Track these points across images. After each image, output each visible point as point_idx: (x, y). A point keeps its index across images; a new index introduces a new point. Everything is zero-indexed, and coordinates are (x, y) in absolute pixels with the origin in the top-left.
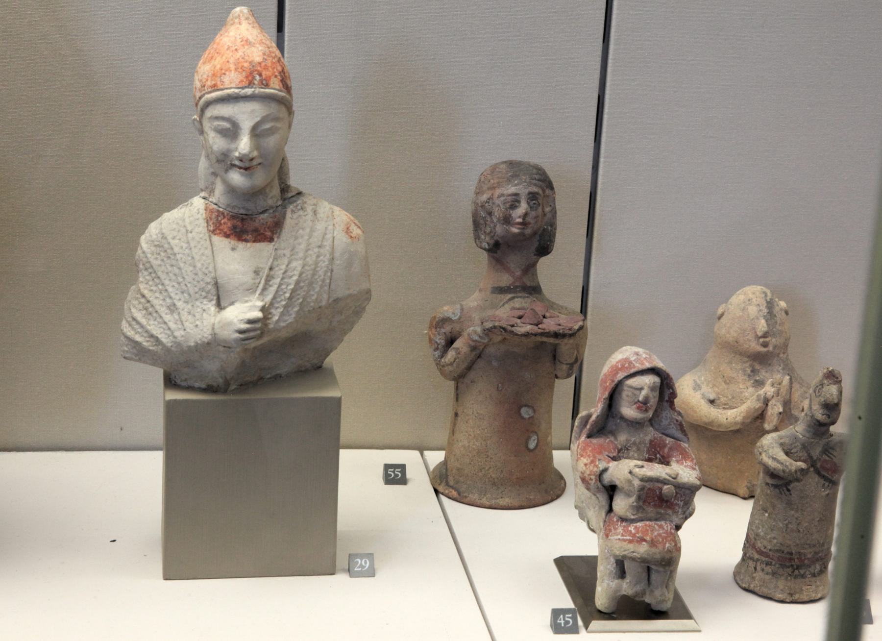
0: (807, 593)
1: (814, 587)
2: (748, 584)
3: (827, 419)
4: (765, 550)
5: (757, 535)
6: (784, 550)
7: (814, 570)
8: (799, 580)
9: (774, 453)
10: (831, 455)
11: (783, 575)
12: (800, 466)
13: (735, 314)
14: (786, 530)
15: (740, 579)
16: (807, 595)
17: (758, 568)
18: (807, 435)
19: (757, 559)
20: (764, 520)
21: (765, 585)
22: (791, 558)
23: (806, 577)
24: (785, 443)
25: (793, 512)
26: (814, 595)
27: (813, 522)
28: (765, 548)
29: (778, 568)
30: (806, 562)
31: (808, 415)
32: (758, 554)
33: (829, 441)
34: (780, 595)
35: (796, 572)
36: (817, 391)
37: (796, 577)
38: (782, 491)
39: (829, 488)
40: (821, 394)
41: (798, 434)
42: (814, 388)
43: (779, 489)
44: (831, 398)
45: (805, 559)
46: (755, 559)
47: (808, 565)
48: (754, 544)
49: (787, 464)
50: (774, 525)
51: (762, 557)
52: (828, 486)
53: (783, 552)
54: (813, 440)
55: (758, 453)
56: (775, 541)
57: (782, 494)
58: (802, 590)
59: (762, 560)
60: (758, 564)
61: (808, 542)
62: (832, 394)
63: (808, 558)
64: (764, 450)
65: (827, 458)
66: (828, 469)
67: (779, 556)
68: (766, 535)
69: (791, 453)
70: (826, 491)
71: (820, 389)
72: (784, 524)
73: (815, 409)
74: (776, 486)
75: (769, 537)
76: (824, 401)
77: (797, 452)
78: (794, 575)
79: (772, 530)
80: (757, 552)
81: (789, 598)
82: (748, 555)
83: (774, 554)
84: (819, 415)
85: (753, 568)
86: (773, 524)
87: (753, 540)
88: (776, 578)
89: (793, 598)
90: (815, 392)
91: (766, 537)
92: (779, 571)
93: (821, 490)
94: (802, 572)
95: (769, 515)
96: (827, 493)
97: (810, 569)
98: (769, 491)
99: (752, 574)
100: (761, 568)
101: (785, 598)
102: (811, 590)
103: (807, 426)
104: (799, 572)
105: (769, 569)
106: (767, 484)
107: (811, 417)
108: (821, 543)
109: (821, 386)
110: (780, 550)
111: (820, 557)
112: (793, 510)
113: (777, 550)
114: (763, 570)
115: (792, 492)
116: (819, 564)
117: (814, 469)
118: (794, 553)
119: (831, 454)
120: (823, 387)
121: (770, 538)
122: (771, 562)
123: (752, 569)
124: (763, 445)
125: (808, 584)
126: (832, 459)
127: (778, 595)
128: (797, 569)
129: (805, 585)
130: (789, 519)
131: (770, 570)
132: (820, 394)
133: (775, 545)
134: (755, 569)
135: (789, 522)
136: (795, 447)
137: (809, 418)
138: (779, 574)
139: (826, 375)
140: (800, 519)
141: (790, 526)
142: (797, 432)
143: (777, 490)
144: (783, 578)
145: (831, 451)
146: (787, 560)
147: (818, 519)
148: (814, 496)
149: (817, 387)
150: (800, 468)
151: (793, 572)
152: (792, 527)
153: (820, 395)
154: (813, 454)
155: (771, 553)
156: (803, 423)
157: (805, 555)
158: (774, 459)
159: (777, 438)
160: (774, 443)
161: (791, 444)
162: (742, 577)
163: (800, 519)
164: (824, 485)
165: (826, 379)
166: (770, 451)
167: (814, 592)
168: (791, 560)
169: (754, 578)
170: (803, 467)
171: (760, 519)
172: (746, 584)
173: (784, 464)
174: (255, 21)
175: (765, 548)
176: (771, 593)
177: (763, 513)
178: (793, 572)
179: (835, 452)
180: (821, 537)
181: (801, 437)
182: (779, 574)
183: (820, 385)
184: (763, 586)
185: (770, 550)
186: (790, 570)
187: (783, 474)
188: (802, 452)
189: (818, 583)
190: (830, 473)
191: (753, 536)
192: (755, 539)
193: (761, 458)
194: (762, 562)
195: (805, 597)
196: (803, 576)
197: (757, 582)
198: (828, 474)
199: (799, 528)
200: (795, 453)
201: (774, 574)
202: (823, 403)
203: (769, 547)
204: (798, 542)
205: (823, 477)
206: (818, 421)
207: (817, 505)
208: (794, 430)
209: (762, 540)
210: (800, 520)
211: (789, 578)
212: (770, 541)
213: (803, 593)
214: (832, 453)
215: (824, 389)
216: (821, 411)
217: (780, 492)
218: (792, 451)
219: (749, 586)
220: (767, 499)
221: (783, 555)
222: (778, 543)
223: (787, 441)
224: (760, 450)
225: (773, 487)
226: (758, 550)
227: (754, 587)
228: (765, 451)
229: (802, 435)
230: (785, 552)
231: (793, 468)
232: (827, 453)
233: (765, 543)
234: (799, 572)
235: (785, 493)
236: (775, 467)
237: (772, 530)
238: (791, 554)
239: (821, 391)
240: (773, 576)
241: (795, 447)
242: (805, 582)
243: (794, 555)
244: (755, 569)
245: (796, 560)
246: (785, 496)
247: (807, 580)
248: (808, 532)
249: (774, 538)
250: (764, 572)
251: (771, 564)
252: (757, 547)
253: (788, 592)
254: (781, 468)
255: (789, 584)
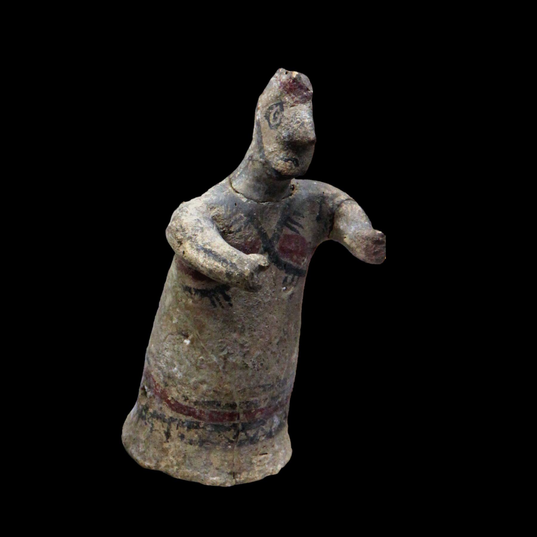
0: (260, 468)
1: (270, 455)
2: (154, 462)
3: (294, 167)
4: (186, 404)
5: (169, 377)
6: (221, 402)
7: (271, 427)
8: (245, 449)
9: (207, 241)
10: (295, 226)
11: (218, 444)
12: (256, 262)
13: (306, 106)
14: (224, 368)
15: (137, 451)
16: (260, 471)
17: (174, 433)
18: (255, 196)
19: (171, 418)
20: (181, 352)
21: (187, 461)
22: (232, 413)
23: (258, 440)
24: (218, 216)
25: (235, 335)
26: (271, 469)
27: (269, 346)
28: (186, 399)
29: (211, 432)
30: (258, 415)
31: (257, 160)
32: (173, 410)
33: (292, 201)
34: (215, 479)
35: (242, 435)
36: (272, 117)
37: (241, 444)
38: (215, 300)
39: (294, 283)
40: (281, 122)
41: (239, 195)
42: (265, 109)
43: (211, 298)
44: (302, 130)
45: (257, 411)
46: (166, 418)
47: (261, 421)
48: (163, 392)
49: (234, 261)
51: (181, 415)
52: (293, 280)
53: (219, 405)
54: (264, 204)
55: (175, 242)
56: (205, 387)
57: (215, 306)
58: (252, 463)
59: (180, 420)
60: (174, 426)
61: (262, 382)
62: (303, 124)
64: (187, 235)
65: (290, 232)
66: (291, 251)
67: (212, 412)
68: (188, 378)
69: (231, 232)
70: (289, 290)
71: (277, 112)
72: (221, 357)
73: (270, 150)
74: (203, 293)
75: (193, 380)
76: (289, 136)
77: (240, 230)
79: (198, 368)
80: (171, 406)
81: (229, 480)
82: (151, 410)
83: (203, 410)
84: (280, 162)
85: (163, 433)
86: (201, 357)
87: (162, 385)
88: (206, 449)
89: (238, 480)
91: (187, 380)
93: (280, 290)
94: (251, 433)
95: (192, 342)
96: (290, 292)
97: (264, 427)
98: (190, 302)
99: (162, 443)
100: (179, 432)
101: (222, 481)
102: (266, 462)
103: (253, 180)
104: (246, 434)
105: (194, 435)
106: (187, 289)
107: (264, 165)
108: (282, 379)
109: (278, 107)
110: (214, 402)
111: (280, 403)
112: (235, 331)
113: (208, 402)
114: (182, 437)
115: (233, 302)
116: (278, 416)
117: (270, 255)
118: (238, 405)
119: (297, 224)
120: (282, 110)
121: (195, 383)
122: (198, 424)
123: (160, 434)
124: (184, 225)
125: (261, 452)
126: (298, 232)
127: (211, 478)
128: (243, 430)
129: (256, 455)
130: (229, 348)
131: (196, 436)
132: (278, 122)
133: (204, 394)
134: (168, 435)
135: (228, 353)
136: (236, 221)
137: (258, 166)
138: (212, 443)
139: (288, 87)
140: (246, 345)
141: (231, 359)
142: (237, 192)
143: (207, 300)
144: (218, 448)
145: (294, 218)
146: (227, 418)
147: (277, 340)
148: (270, 303)
149: (271, 108)
150: (257, 265)
151: (236, 437)
152: (234, 361)
153: (278, 125)
154: (266, 229)
155: (197, 409)
156: (246, 174)
157: (256, 406)
158: (209, 252)
159: (204, 209)
160: (202, 221)
161: (230, 217)
162: (141, 449)
163: (246, 345)
164: (285, 280)
165: (288, 93)
166: (199, 238)
168: (232, 416)
169: (165, 451)
170: (262, 263)
171: (174, 351)
172: (151, 461)
173: (228, 261)
175: (186, 399)
176: (198, 476)
177: (180, 339)
178: (236, 437)
180: (283, 369)
181: (244, 200)
182: (212, 443)
183: (277, 105)
184: (183, 464)
185: (196, 403)
186: (230, 434)
187: (226, 280)
189: (277, 447)
190: (295, 257)
191: (162, 378)
192: (166, 385)
194: (181, 424)
195: (257, 475)
196: (253, 441)
197: (171, 458)
198: (291, 259)
199: (246, 361)
200: (237, 232)
201: (202, 442)
202: (287, 140)
203: (194, 399)
204: (244, 384)
206: (277, 172)
207: (275, 317)
208: (230, 188)
209: (179, 386)
210: (248, 347)
211: (230, 447)
212: (195, 388)
213: (253, 469)
214: (296, 221)
215: (285, 113)
216: (282, 155)
217: (213, 303)
218: (232, 229)
219: (157, 465)
220: (188, 316)
221: (220, 410)
222: (210, 391)
223: (221, 210)
224: (179, 236)
226: (172, 403)
227: (167, 466)
228: (190, 238)
230: (223, 404)
231: (247, 269)
232: (289, 223)
233: (186, 391)
234: (246, 434)
235: (220, 304)
236: (211, 268)
237: (198, 368)
238: (233, 406)
239: (279, 117)
240: (201, 446)
241: (236, 221)
242: (256, 450)
243: (238, 408)
244: (168, 435)
245: (241, 416)
246: (220, 309)
247: (259, 445)
248: (262, 364)
249: (203, 382)
250: (185, 440)
251: (197, 427)
252: (169, 399)
253: (229, 471)
254: (224, 269)
255: (230, 457)
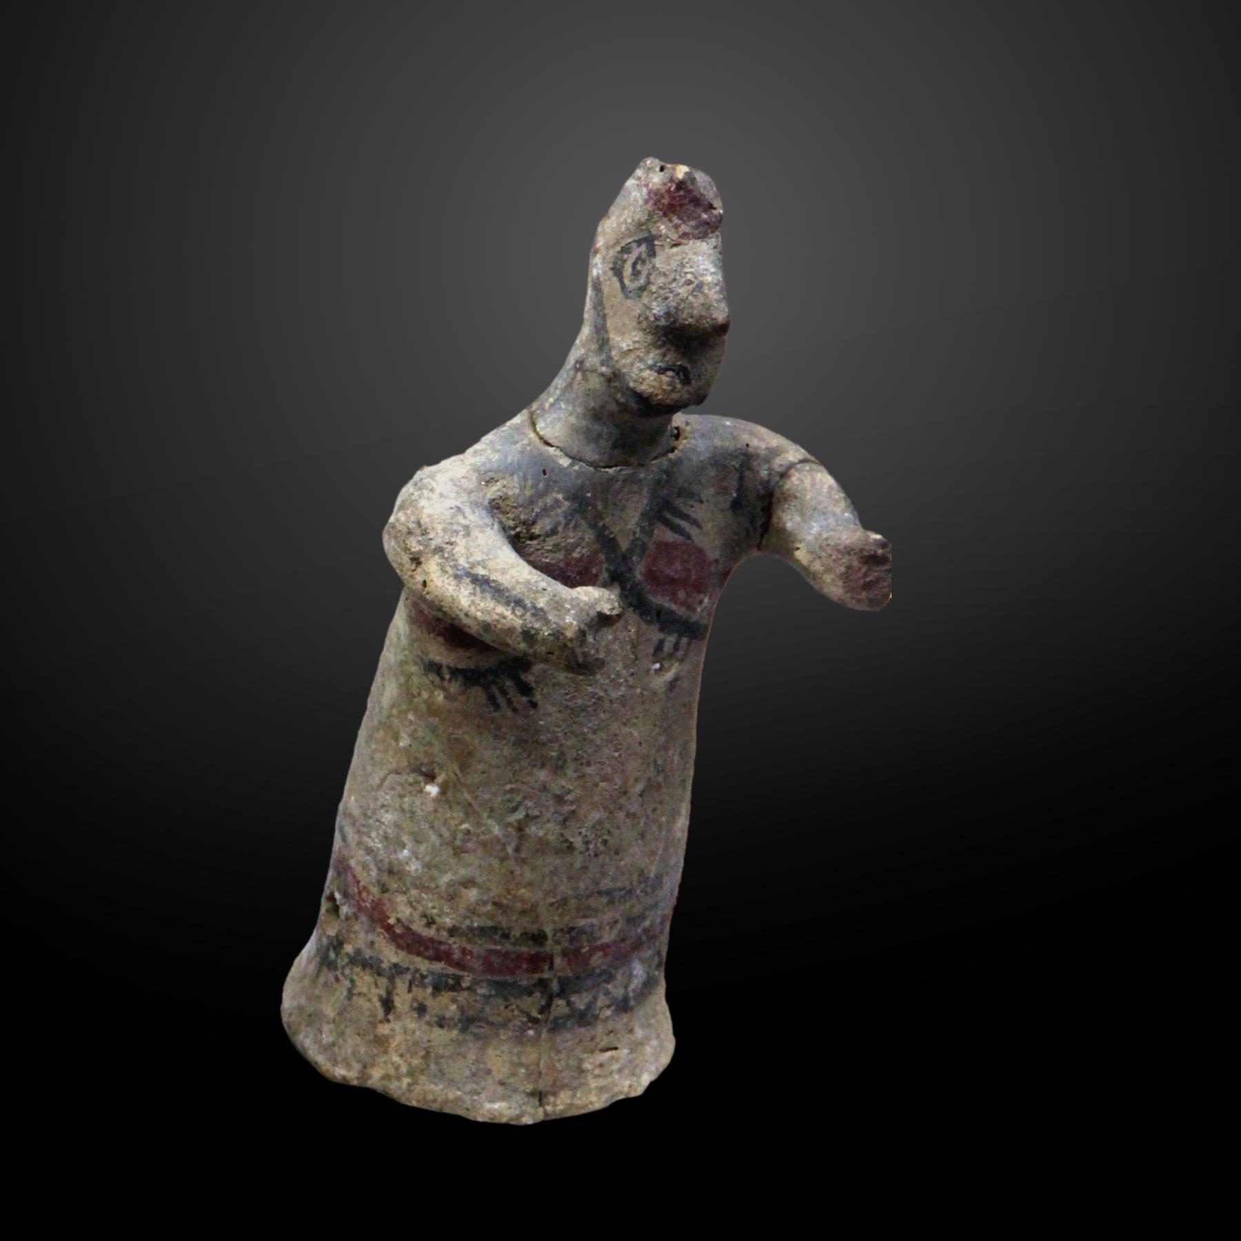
1: (624, 1052)
2: (357, 1067)
3: (679, 386)
4: (430, 933)
5: (391, 872)
6: (510, 929)
7: (626, 987)
8: (566, 1039)
9: (478, 557)
10: (683, 523)
11: (504, 1025)
12: (592, 606)
14: (517, 849)
15: (317, 1042)
16: (601, 1089)
17: (402, 1000)
18: (590, 453)
19: (395, 965)
20: (419, 813)
21: (433, 1066)
22: (537, 954)
23: (596, 1017)
24: (505, 498)
25: (543, 775)
26: (627, 1083)
27: (623, 801)
28: (430, 922)
29: (487, 998)
30: (597, 960)
31: (594, 371)
32: (399, 946)
33: (674, 464)
34: (496, 1106)
35: (560, 1006)
36: (628, 270)
37: (556, 1026)
38: (497, 692)
39: (680, 653)
40: (648, 283)
41: (551, 450)
42: (612, 253)
43: (486, 688)
44: (697, 301)
45: (593, 950)
46: (385, 965)
47: (603, 972)
48: (377, 905)
49: (542, 603)
50: (468, 832)
51: (418, 959)
52: (676, 647)
53: (506, 936)
54: (611, 471)
55: (405, 559)
56: (473, 894)
57: (497, 707)
59: (417, 970)
60: (401, 985)
61: (606, 883)
62: (700, 287)
63: (604, 948)
64: (433, 544)
65: (670, 536)
66: (672, 581)
67: (491, 951)
68: (435, 873)
69: (533, 537)
70: (667, 670)
71: (639, 259)
72: (510, 824)
73: (624, 346)
74: (470, 677)
75: (445, 879)
76: (668, 314)
77: (554, 532)
78: (551, 1018)
79: (458, 852)
80: (395, 938)
81: (529, 1109)
83: (468, 947)
84: (646, 373)
85: (376, 1000)
86: (465, 826)
87: (375, 890)
88: (477, 1037)
89: (549, 1108)
90: (617, 271)
91: (433, 879)
92: (487, 1009)
94: (580, 1002)
95: (443, 791)
96: (669, 676)
98: (440, 697)
99: (373, 1025)
100: (415, 999)
102: (615, 1067)
103: (585, 416)
104: (569, 1004)
105: (447, 1005)
106: (433, 668)
107: (609, 380)
108: (652, 875)
109: (643, 247)
110: (495, 929)
111: (646, 931)
113: (482, 929)
114: (421, 1009)
115: (538, 697)
116: (642, 961)
117: (623, 589)
118: (550, 935)
119: (685, 517)
120: (652, 253)
121: (450, 884)
122: (458, 980)
123: (370, 1004)
124: (425, 520)
125: (603, 1044)
126: (688, 537)
127: (488, 1106)
128: (562, 993)
129: (592, 1052)
130: (530, 804)
131: (453, 1007)
132: (642, 281)
133: (472, 912)
134: (388, 1004)
135: (527, 816)
136: (546, 510)
137: (595, 382)
138: (491, 1024)
139: (666, 201)
140: (569, 797)
141: (533, 830)
142: (548, 444)
143: (477, 693)
144: (504, 1035)
145: (679, 503)
146: (525, 966)
147: (640, 787)
149: (626, 250)
150: (593, 613)
151: (545, 1009)
152: (541, 833)
153: (642, 289)
154: (616, 529)
155: (455, 944)
156: (568, 402)
157: (592, 937)
158: (482, 583)
159: (471, 484)
160: (467, 510)
161: (532, 502)
162: (327, 1038)
163: (569, 797)
164: (659, 647)
165: (665, 215)
167: (626, 1071)
168: (536, 962)
169: (381, 1042)
170: (606, 608)
171: (403, 810)
172: (348, 1066)
173: (528, 602)
174: (462, 963)
175: (430, 922)
176: (458, 1099)
177: (417, 782)
178: (545, 1009)
179: (696, 504)
180: (653, 853)
181: (565, 462)
182: (491, 1024)
183: (639, 243)
184: (422, 1072)
185: (453, 931)
186: (532, 1004)
187: (523, 646)
188: (576, 526)
189: (639, 1033)
190: (681, 594)
191: (374, 873)
192: (384, 889)
193: (419, 578)
194: (418, 980)
195: (594, 1099)
196: (584, 1018)
197: (396, 1058)
198: (674, 598)
199: (568, 834)
200: (548, 535)
201: (467, 1022)
202: (663, 322)
203: (448, 921)
204: (564, 888)
205: (663, 620)
206: (641, 398)
207: (635, 734)
208: (532, 435)
209: (414, 892)
210: (572, 803)
211: (531, 1032)
212: (452, 897)
214: (685, 510)
215: (658, 262)
216: (652, 357)
217: (492, 699)
218: (536, 530)
219: (364, 1075)
220: (433, 730)
221: (508, 947)
222: (485, 903)
223: (511, 486)
224: (414, 544)
225: (460, 678)
226: (398, 931)
227: (387, 1077)
228: (439, 550)
229: (567, 455)
230: (516, 933)
231: (571, 622)
232: (669, 516)
233: (430, 903)
234: (569, 1004)
235: (509, 702)
236: (488, 619)
237: (458, 852)
238: (540, 938)
239: (644, 269)
240: (464, 1030)
241: (546, 510)
242: (592, 1039)
243: (549, 942)
244: (388, 1004)
245: (558, 961)
246: (510, 713)
247: (600, 1029)
248: (605, 842)
249: (469, 883)
250: (427, 1018)
251: (456, 986)
252: (392, 921)
253: (529, 1088)
254: (518, 623)
255: (531, 1056)
